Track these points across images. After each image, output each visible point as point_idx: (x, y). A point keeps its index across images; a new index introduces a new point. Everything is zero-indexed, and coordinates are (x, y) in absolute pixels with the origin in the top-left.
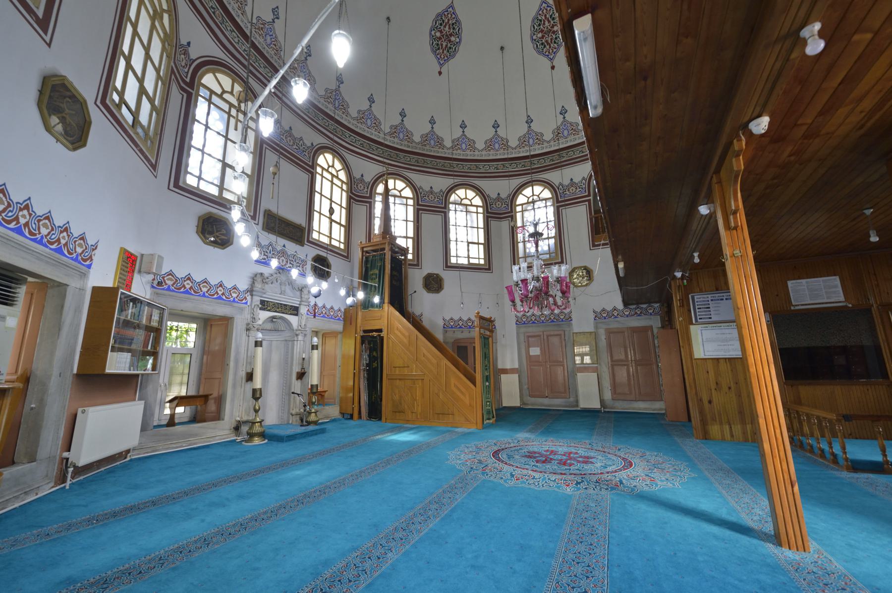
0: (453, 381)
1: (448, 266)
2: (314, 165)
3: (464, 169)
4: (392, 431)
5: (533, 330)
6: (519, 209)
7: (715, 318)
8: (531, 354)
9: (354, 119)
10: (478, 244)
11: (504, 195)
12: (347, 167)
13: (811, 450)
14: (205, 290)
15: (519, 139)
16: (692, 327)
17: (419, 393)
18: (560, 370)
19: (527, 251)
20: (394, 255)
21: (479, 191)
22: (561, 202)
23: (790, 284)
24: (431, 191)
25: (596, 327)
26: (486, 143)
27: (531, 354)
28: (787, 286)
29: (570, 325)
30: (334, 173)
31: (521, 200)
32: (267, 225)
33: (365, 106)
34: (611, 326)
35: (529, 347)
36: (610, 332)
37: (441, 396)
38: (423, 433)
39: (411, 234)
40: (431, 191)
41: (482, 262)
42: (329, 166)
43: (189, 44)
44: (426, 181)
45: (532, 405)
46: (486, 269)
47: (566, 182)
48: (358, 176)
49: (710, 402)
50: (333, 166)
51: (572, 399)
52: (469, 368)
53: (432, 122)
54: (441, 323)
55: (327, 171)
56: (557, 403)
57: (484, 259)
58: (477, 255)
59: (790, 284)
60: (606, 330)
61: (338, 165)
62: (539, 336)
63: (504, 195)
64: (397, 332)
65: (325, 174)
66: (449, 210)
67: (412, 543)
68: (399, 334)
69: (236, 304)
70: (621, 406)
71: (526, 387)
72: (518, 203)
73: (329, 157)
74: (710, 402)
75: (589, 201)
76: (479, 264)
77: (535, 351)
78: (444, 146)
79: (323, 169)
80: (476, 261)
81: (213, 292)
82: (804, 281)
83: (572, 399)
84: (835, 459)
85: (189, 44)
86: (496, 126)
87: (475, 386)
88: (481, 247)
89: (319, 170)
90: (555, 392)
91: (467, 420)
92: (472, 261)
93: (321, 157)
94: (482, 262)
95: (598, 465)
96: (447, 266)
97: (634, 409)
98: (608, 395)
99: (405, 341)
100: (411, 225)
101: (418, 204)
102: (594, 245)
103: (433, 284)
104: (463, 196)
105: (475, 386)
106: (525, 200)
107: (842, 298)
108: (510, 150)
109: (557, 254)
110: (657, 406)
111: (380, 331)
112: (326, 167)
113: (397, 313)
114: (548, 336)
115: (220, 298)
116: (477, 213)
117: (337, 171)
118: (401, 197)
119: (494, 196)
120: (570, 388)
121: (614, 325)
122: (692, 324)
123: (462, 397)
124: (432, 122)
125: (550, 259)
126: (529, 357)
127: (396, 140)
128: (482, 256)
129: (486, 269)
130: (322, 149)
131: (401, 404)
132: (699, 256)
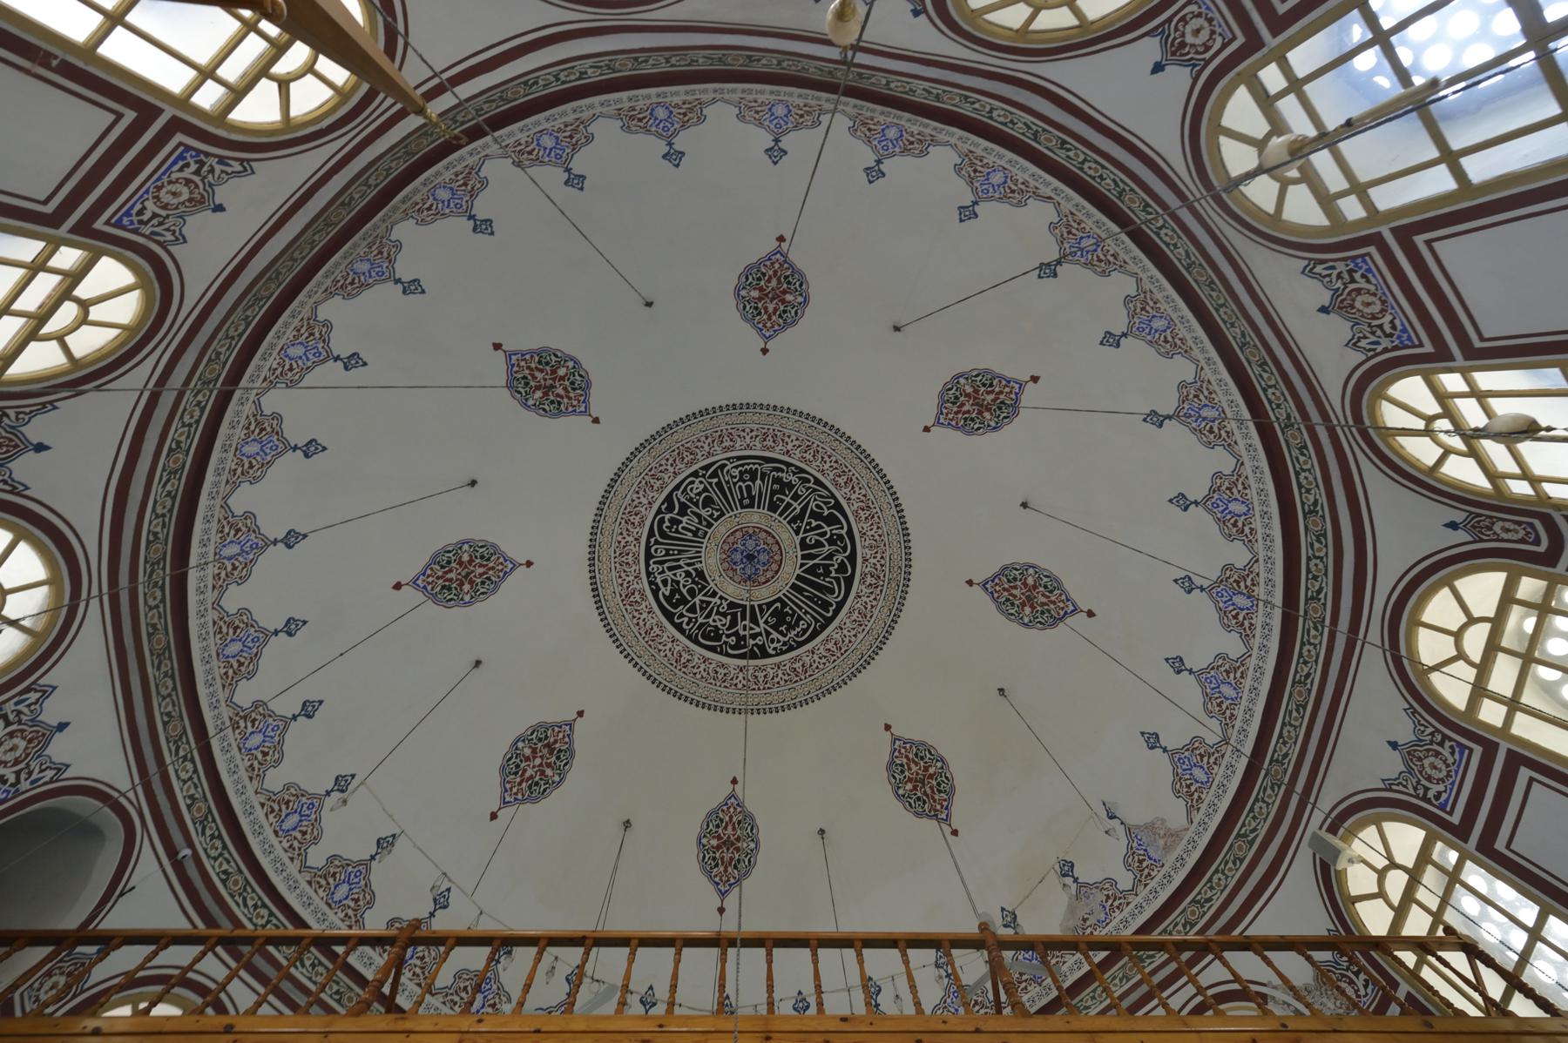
2: (96, 239)
11: (1404, 731)
12: (83, 378)
28: (132, 108)
30: (54, 325)
40: (203, 201)
42: (85, 305)
43: (219, 208)
44: (252, 200)
48: (35, 430)
50: (83, 320)
53: (291, 627)
55: (65, 294)
61: (87, 342)
63: (1404, 731)
65: (45, 284)
73: (126, 309)
79: (74, 277)
85: (219, 208)
86: (1153, 741)
89: (68, 257)
93: (125, 276)
112: (84, 290)
116: (207, 73)
117: (60, 338)
119: (1393, 765)
127: (239, 433)
130: (159, 280)
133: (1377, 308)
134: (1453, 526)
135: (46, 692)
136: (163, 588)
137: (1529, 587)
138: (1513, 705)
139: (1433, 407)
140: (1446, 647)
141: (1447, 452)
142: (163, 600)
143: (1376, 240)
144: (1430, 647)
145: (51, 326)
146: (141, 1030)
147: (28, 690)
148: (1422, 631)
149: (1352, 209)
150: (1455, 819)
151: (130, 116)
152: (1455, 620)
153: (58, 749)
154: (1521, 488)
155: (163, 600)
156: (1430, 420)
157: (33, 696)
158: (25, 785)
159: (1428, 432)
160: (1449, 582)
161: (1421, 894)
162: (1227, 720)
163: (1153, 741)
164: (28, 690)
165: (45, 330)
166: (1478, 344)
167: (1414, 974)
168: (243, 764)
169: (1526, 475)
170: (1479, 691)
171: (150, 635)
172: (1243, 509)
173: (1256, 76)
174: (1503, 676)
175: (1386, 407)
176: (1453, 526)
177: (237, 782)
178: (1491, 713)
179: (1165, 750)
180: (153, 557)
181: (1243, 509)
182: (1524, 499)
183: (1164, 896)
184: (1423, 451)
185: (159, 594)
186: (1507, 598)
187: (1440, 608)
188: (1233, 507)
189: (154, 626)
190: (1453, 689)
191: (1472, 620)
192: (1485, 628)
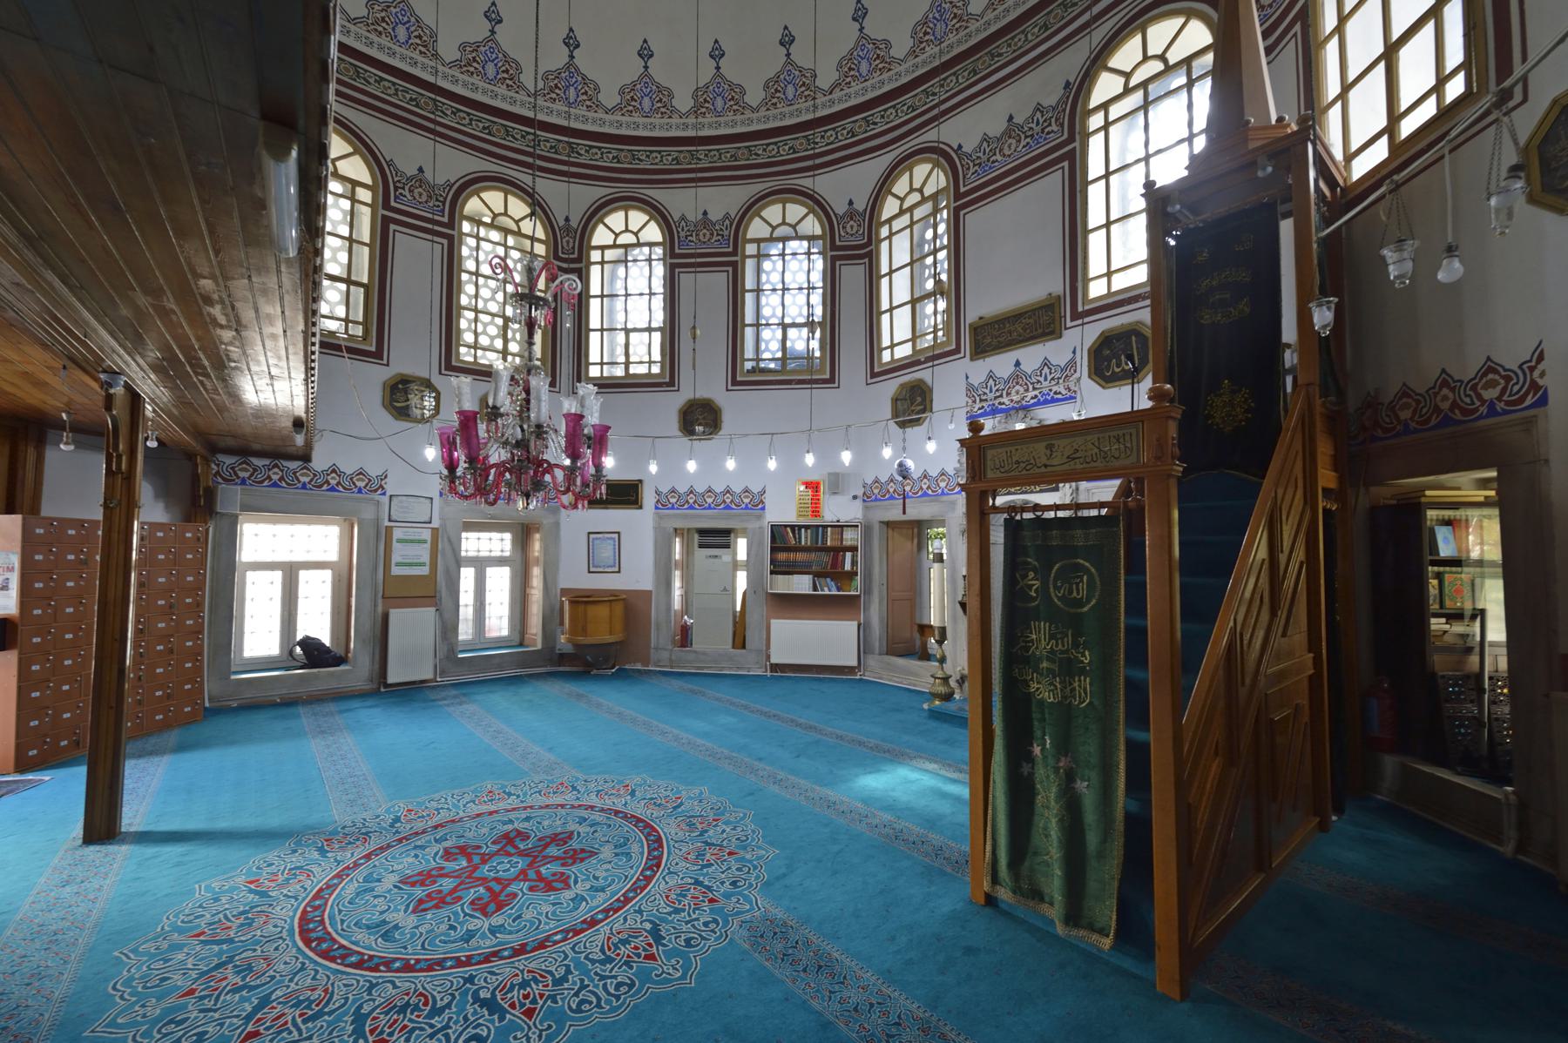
3: (629, 166)
6: (751, 249)
9: (452, 65)
10: (649, 330)
14: (709, 500)
15: (621, 92)
19: (789, 344)
21: (658, 213)
24: (705, 221)
26: (766, 86)
31: (757, 229)
32: (1052, 333)
33: (480, 30)
39: (659, 318)
40: (705, 221)
41: (656, 369)
53: (645, 53)
57: (662, 363)
58: (646, 354)
66: (745, 257)
67: (562, 869)
69: (945, 498)
72: (594, 243)
78: (674, 110)
80: (641, 370)
86: (787, 40)
88: (657, 336)
92: (632, 370)
94: (656, 369)
96: (671, 383)
100: (658, 303)
101: (557, 257)
104: (776, 220)
106: (765, 232)
108: (821, 100)
111: (701, 546)
115: (925, 494)
118: (519, 234)
124: (645, 53)
128: (657, 356)
133: (1007, 152)
134: (567, 219)
137: (659, 251)
138: (602, 263)
139: (928, 191)
140: (619, 227)
141: (902, 200)
143: (1071, 139)
144: (616, 220)
148: (805, 211)
149: (1096, 121)
152: (634, 227)
154: (884, 232)
156: (920, 191)
159: (912, 190)
161: (607, 252)
162: (696, 111)
163: (787, 40)
167: (745, 257)
169: (891, 235)
170: (603, 248)
172: (790, 96)
174: (610, 255)
175: (928, 167)
176: (567, 219)
178: (595, 256)
179: (788, 55)
181: (790, 96)
182: (878, 233)
183: (458, 90)
184: (901, 186)
186: (651, 245)
187: (637, 218)
188: (790, 89)
190: (601, 236)
191: (636, 234)
192: (634, 241)
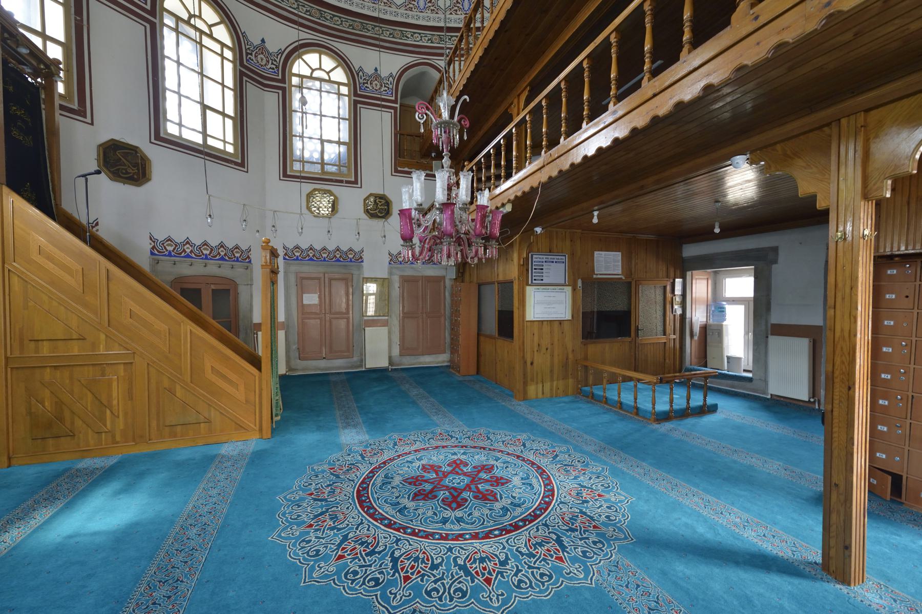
0: (209, 362)
1: (159, 136)
4: (51, 499)
5: (308, 269)
7: (545, 281)
8: (305, 302)
13: (606, 401)
16: (528, 288)
17: (117, 393)
18: (342, 323)
20: (13, 63)
22: (361, 95)
23: (596, 253)
25: (391, 273)
27: (305, 302)
29: (360, 268)
34: (406, 274)
35: (302, 293)
36: (407, 281)
37: (179, 392)
38: (150, 483)
43: (263, 41)
45: (303, 370)
46: (236, 164)
47: (370, 71)
49: (532, 364)
51: (355, 359)
52: (240, 341)
54: (147, 246)
56: (337, 365)
59: (596, 253)
60: (401, 277)
62: (319, 279)
64: (35, 257)
68: (50, 266)
70: (409, 362)
71: (294, 347)
74: (532, 364)
75: (395, 109)
76: (224, 152)
77: (311, 299)
81: (214, 253)
82: (603, 253)
83: (355, 359)
84: (637, 411)
85: (263, 41)
87: (259, 369)
90: (333, 353)
91: (240, 427)
95: (521, 488)
97: (420, 363)
98: (396, 351)
99: (73, 282)
102: (396, 171)
103: (124, 163)
105: (259, 369)
107: (620, 272)
109: (349, 170)
110: (441, 359)
113: (34, 212)
114: (330, 280)
115: (311, 260)
120: (353, 343)
121: (409, 272)
122: (528, 285)
123: (230, 389)
125: (340, 173)
126: (301, 306)
129: (236, 164)
131: (61, 419)
132: (598, 216)
135: (361, 69)
136: (334, 16)
142: (340, 18)
145: (207, 30)
146: (678, 84)
147: (358, 74)
150: (280, 77)
151: (359, 105)
153: (384, 73)
155: (340, 18)
157: (361, 73)
158: (391, 86)
160: (300, 57)
164: (358, 74)
165: (208, 32)
166: (280, 92)
168: (429, 14)
171: (353, 29)
173: (255, 324)
177: (434, 20)
180: (318, 15)
185: (336, 18)
189: (350, 25)
